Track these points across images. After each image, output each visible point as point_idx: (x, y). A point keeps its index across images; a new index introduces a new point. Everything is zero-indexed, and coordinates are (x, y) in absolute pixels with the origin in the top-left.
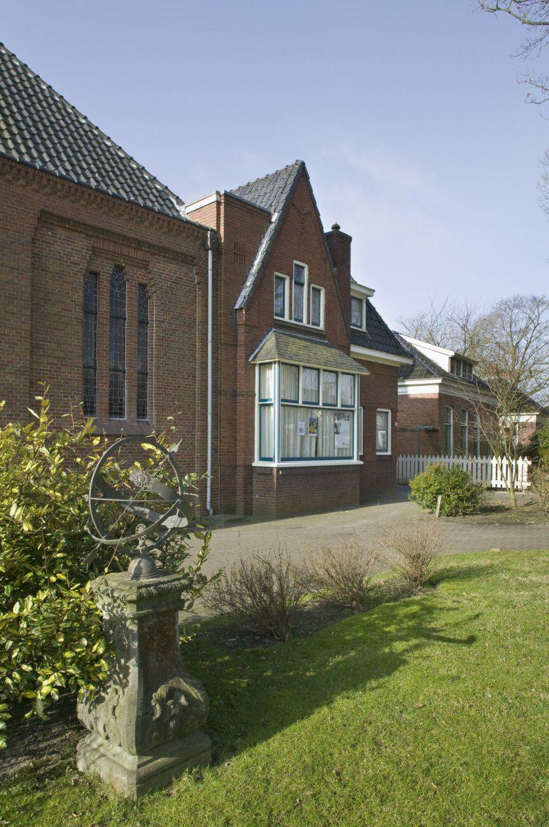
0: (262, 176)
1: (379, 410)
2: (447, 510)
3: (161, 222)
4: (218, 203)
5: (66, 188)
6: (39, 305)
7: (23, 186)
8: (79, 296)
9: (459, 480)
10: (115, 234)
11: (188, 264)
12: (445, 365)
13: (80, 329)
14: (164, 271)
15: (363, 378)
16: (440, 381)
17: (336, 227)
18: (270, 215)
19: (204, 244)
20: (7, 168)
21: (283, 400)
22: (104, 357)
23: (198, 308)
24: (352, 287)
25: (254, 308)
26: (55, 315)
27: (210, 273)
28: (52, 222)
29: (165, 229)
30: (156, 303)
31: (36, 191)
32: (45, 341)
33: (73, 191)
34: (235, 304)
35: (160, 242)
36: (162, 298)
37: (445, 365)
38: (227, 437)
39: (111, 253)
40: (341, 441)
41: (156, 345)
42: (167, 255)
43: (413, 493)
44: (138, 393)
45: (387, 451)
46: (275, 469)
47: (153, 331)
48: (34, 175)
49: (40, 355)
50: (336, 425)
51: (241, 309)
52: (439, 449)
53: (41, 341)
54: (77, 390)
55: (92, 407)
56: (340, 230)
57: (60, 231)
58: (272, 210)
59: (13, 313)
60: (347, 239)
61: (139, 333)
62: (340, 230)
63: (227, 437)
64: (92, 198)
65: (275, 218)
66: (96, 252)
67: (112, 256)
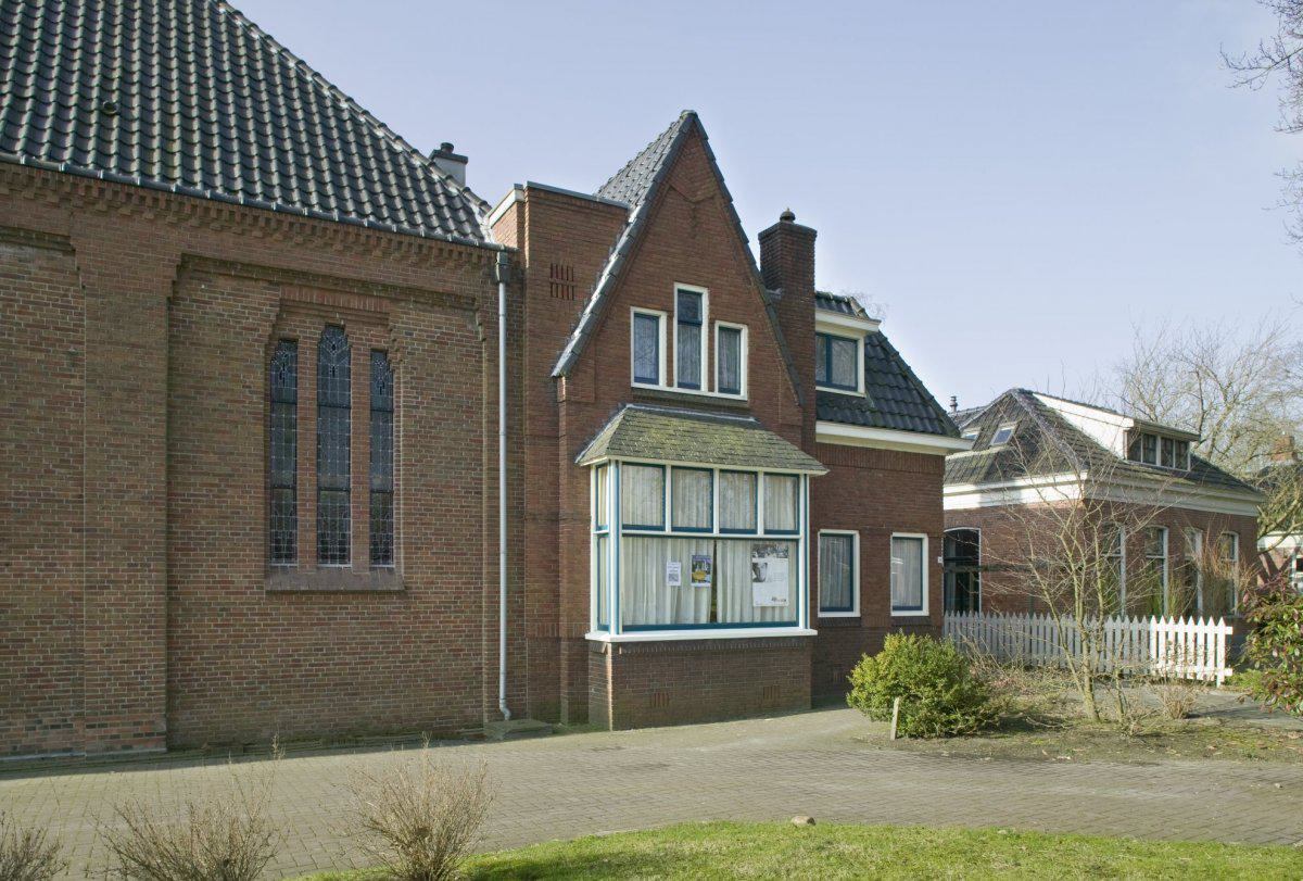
1: (895, 534)
2: (911, 726)
3: (404, 248)
5: (225, 215)
6: (186, 397)
7: (151, 221)
8: (257, 379)
10: (318, 275)
11: (465, 309)
13: (259, 429)
14: (415, 325)
18: (626, 211)
19: (491, 275)
20: (122, 197)
21: (625, 527)
22: (307, 469)
25: (586, 372)
26: (215, 410)
27: (502, 320)
28: (206, 269)
29: (414, 258)
30: (404, 377)
31: (172, 225)
32: (197, 452)
33: (237, 218)
34: (553, 367)
35: (404, 280)
36: (415, 369)
38: (539, 591)
39: (316, 307)
40: (763, 595)
41: (404, 445)
42: (422, 300)
43: (855, 693)
44: (372, 524)
45: (920, 608)
46: (610, 645)
47: (400, 423)
48: (168, 202)
49: (189, 473)
50: (755, 567)
51: (560, 377)
53: (192, 451)
54: (255, 523)
55: (289, 549)
56: (796, 222)
57: (221, 281)
58: (632, 206)
59: (137, 413)
60: (808, 236)
61: (375, 430)
62: (796, 222)
63: (539, 591)
64: (273, 224)
65: (632, 218)
67: (319, 310)
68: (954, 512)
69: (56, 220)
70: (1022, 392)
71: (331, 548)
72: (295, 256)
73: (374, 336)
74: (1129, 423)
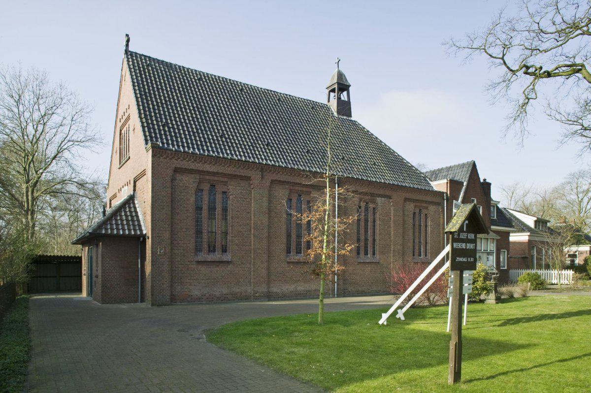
0: (457, 164)
4: (447, 183)
9: (538, 277)
12: (532, 225)
15: (497, 240)
16: (529, 234)
17: (485, 180)
18: (463, 183)
23: (441, 220)
24: (492, 202)
27: (445, 208)
37: (532, 225)
45: (505, 267)
47: (429, 229)
50: (487, 258)
52: (529, 266)
60: (489, 185)
65: (465, 184)
66: (415, 206)
68: (515, 243)
69: (388, 193)
72: (199, 166)
73: (307, 198)
74: (535, 219)
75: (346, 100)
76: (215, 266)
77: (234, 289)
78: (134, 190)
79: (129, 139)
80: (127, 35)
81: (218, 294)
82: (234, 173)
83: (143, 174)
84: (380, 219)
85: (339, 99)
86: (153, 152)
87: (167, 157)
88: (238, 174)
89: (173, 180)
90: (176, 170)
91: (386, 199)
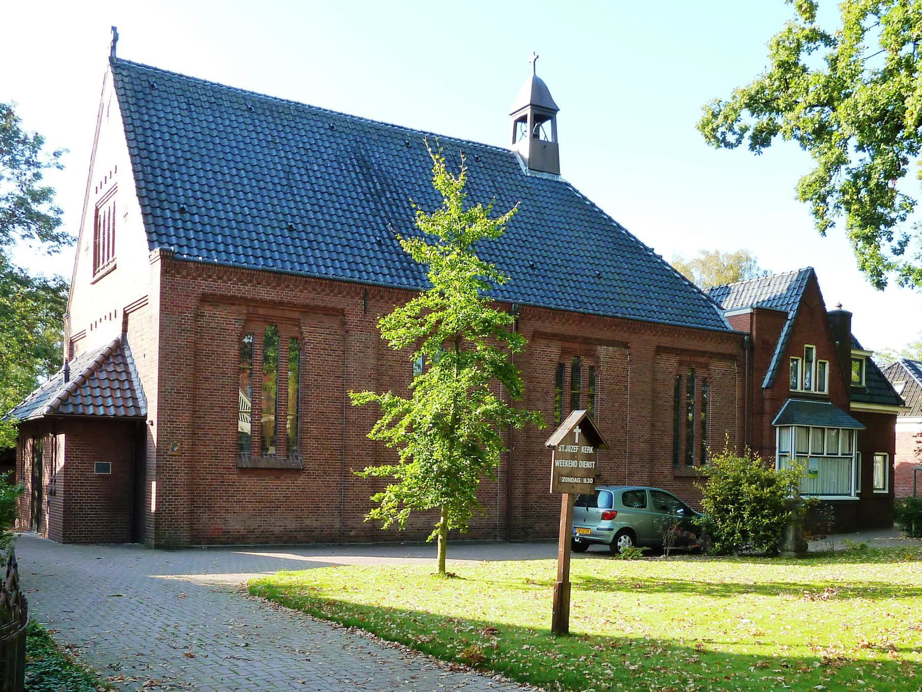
18: (787, 314)
45: (884, 489)
70: (906, 361)
71: (689, 461)
72: (245, 290)
75: (550, 140)
76: (273, 477)
77: (308, 522)
78: (125, 330)
79: (114, 229)
80: (114, 29)
81: (277, 530)
82: (312, 303)
83: (143, 302)
84: (602, 388)
85: (535, 136)
86: (163, 265)
87: (188, 274)
88: (320, 304)
89: (198, 316)
90: (205, 299)
91: (616, 348)
